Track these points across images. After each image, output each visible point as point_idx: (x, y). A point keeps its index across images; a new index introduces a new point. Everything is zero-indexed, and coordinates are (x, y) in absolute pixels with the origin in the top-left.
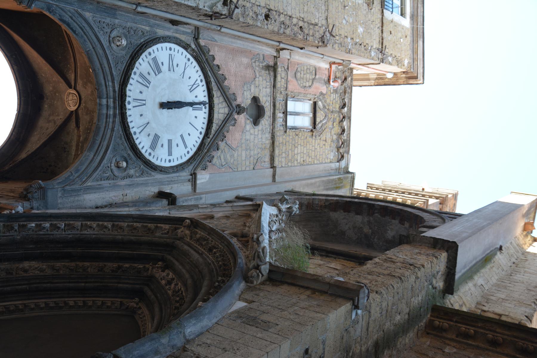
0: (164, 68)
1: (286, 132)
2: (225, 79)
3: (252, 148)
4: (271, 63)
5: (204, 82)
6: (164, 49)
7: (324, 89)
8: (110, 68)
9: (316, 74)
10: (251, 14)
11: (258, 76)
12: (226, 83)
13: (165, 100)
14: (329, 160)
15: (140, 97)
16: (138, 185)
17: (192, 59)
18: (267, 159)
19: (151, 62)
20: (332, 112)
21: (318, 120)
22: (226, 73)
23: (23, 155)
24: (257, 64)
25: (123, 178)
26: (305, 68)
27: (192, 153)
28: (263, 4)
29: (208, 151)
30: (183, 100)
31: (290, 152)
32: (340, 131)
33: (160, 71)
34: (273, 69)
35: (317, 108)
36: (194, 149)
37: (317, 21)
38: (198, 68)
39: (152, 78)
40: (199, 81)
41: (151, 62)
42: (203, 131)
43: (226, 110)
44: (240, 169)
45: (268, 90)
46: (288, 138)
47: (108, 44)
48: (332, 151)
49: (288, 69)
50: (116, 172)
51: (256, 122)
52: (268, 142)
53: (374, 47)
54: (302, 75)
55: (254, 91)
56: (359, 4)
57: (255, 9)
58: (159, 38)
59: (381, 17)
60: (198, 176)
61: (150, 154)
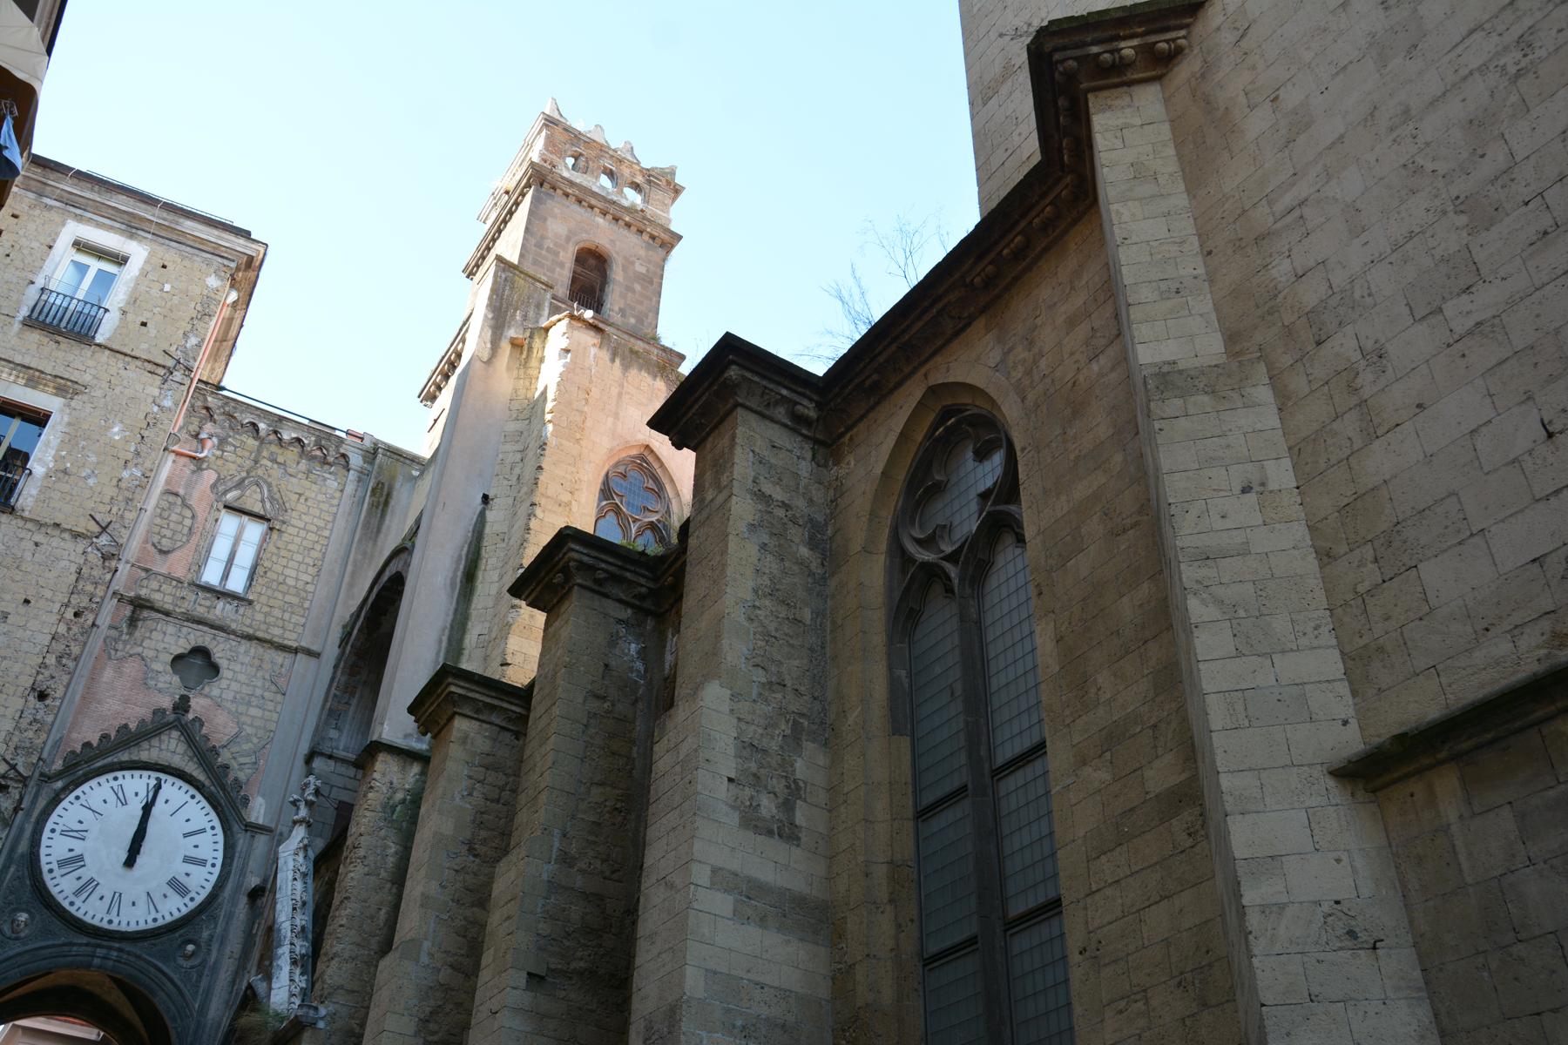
0: (79, 847)
1: (250, 603)
2: (126, 726)
3: (248, 690)
4: (127, 610)
5: (119, 774)
6: (50, 843)
7: (209, 476)
8: (53, 946)
9: (176, 495)
10: (30, 734)
11: (139, 650)
12: (133, 726)
13: (124, 856)
14: (338, 494)
15: (107, 900)
16: (226, 930)
17: (78, 792)
18: (280, 657)
19: (64, 871)
20: (256, 462)
21: (258, 509)
22: (117, 723)
23: (145, 1035)
24: (120, 646)
25: (209, 952)
26: (158, 521)
27: (217, 823)
28: (20, 703)
29: (224, 789)
30: (134, 829)
31: (288, 598)
32: (297, 450)
33: (80, 858)
34: (140, 606)
35: (236, 505)
36: (213, 815)
37: (74, 568)
38: (93, 783)
39: (86, 874)
40: (115, 784)
41: (64, 871)
42: (193, 791)
43: (175, 734)
44: (273, 727)
45: (171, 629)
46: (263, 599)
47: (18, 943)
48: (325, 479)
49: (147, 570)
50: (196, 961)
51: (214, 669)
52: (255, 649)
53: (156, 392)
54: (168, 533)
55: (162, 665)
56: (69, 424)
57: (24, 723)
58: (32, 853)
59: (107, 352)
60: (253, 820)
61: (192, 899)
